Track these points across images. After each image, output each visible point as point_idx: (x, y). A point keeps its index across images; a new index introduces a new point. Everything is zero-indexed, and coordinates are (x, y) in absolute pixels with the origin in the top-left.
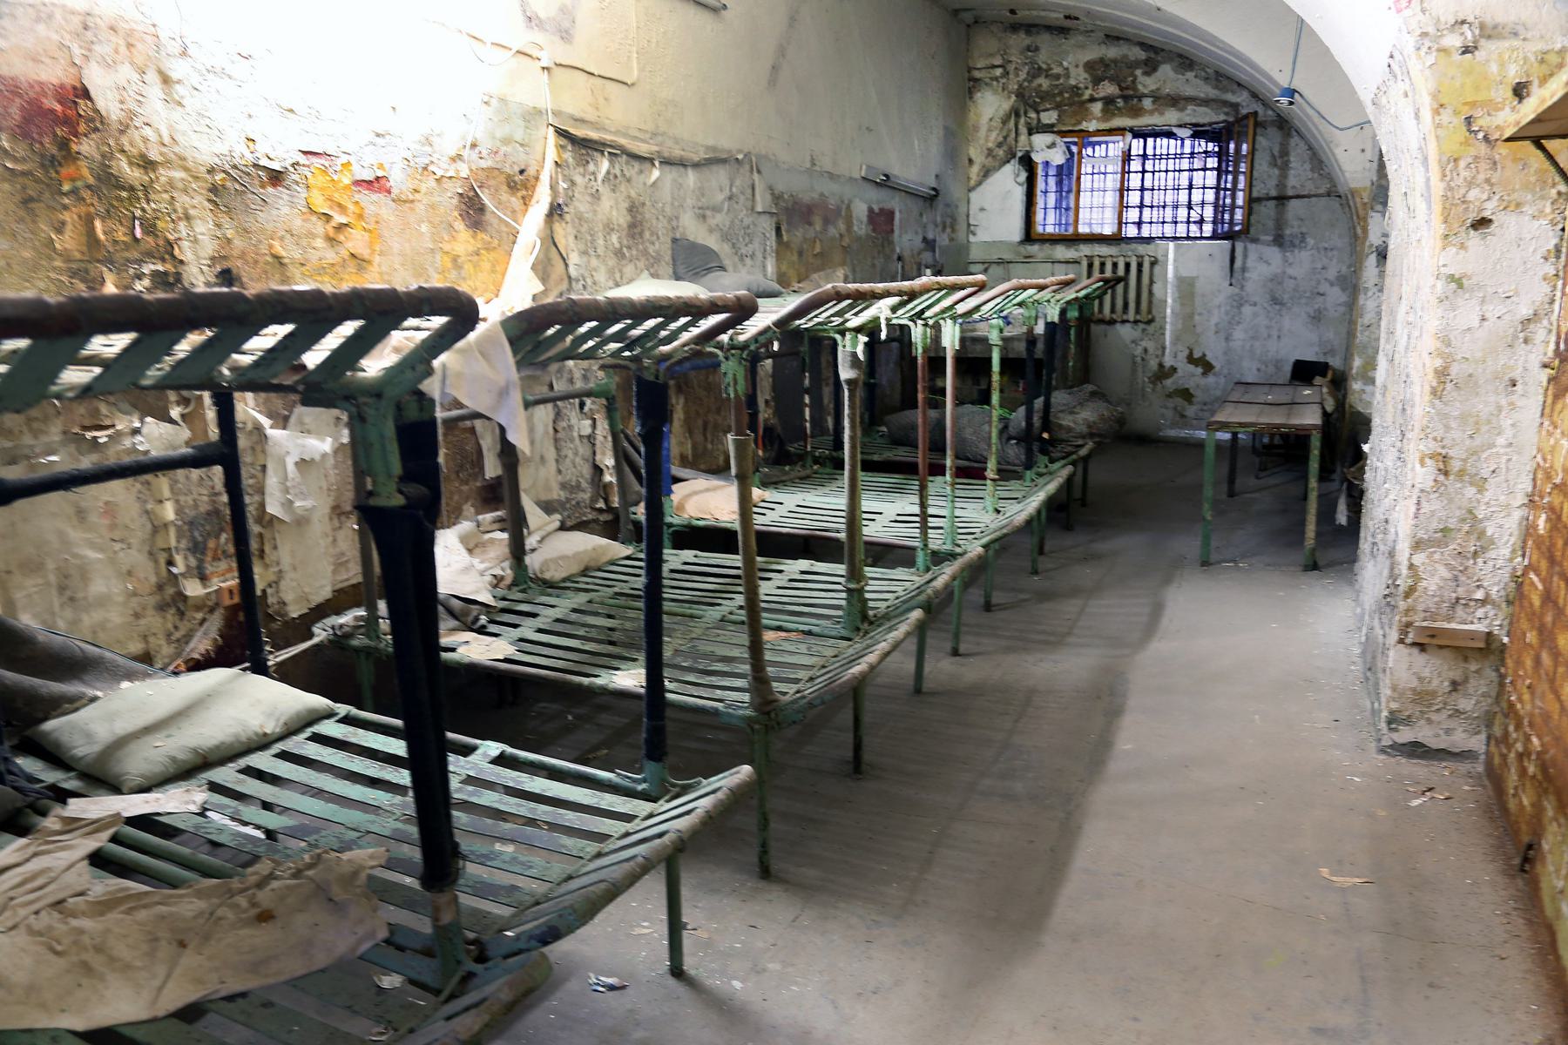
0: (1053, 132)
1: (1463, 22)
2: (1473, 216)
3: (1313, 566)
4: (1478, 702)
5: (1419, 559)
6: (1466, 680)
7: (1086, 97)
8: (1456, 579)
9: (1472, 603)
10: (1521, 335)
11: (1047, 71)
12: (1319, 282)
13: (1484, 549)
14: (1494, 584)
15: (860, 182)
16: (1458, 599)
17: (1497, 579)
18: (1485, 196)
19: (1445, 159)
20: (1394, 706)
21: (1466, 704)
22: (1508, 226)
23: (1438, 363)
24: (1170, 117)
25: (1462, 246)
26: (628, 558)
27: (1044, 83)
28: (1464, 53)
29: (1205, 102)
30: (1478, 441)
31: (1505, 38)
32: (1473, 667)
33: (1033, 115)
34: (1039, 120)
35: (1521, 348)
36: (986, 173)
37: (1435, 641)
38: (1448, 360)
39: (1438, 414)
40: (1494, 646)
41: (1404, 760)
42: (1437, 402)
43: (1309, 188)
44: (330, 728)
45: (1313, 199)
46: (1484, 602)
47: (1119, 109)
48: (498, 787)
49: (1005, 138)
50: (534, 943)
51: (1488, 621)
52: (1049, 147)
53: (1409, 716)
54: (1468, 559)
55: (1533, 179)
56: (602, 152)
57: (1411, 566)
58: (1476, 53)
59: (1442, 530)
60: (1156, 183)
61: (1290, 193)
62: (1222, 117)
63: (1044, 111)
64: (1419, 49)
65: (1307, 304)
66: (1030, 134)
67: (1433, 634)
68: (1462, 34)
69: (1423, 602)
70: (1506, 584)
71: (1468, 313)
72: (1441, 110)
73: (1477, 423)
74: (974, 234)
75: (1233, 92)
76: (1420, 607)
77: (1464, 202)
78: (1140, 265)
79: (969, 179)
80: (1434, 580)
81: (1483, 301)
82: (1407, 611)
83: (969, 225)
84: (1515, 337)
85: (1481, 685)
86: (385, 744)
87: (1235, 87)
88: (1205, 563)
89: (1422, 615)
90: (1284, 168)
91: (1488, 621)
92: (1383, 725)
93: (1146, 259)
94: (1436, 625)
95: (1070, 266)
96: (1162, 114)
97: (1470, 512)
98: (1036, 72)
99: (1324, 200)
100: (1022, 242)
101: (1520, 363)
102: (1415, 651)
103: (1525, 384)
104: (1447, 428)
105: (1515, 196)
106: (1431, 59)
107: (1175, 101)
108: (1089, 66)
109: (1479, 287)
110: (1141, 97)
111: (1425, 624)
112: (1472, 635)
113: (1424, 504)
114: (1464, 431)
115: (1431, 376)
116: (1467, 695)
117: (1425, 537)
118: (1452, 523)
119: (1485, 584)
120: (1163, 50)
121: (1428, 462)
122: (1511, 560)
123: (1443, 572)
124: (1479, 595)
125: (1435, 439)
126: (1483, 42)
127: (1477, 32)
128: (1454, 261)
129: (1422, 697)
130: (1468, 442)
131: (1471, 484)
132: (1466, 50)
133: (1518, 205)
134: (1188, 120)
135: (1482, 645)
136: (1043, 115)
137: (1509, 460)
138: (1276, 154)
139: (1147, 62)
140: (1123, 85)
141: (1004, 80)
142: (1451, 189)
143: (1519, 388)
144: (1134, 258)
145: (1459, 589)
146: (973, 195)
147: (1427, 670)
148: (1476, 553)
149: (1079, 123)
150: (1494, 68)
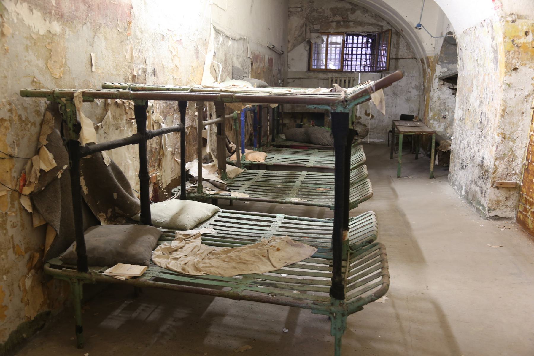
0: (318, 32)
1: (512, 14)
2: (513, 67)
3: (432, 177)
4: (513, 203)
5: (497, 163)
6: (510, 197)
7: (331, 20)
8: (507, 168)
9: (511, 175)
10: (525, 100)
11: (317, 10)
12: (409, 88)
13: (515, 159)
14: (517, 169)
15: (267, 48)
16: (508, 174)
17: (518, 168)
18: (517, 62)
19: (506, 51)
20: (490, 205)
21: (510, 204)
22: (523, 70)
23: (503, 108)
24: (359, 29)
25: (510, 75)
26: (243, 172)
27: (315, 14)
28: (512, 22)
29: (371, 24)
30: (513, 129)
31: (523, 19)
32: (512, 193)
33: (311, 26)
34: (313, 28)
35: (525, 104)
36: (294, 46)
37: (502, 186)
38: (506, 107)
39: (503, 122)
40: (517, 186)
41: (493, 221)
42: (502, 118)
43: (406, 56)
44: (220, 214)
45: (407, 60)
46: (515, 174)
47: (342, 25)
48: (364, 200)
49: (302, 34)
50: (367, 243)
51: (516, 180)
52: (317, 38)
53: (494, 208)
54: (510, 162)
55: (529, 57)
56: (220, 34)
57: (495, 165)
58: (516, 22)
59: (503, 155)
60: (347, 52)
61: (400, 57)
62: (377, 30)
63: (315, 24)
64: (500, 20)
65: (405, 95)
66: (310, 33)
67: (501, 184)
68: (512, 17)
69: (498, 175)
70: (521, 169)
71: (511, 94)
72: (506, 38)
73: (513, 124)
74: (290, 68)
75: (381, 22)
76: (497, 177)
77: (511, 63)
78: (349, 81)
79: (288, 48)
80: (501, 169)
81: (515, 90)
82: (494, 178)
83: (288, 65)
84: (524, 100)
85: (514, 197)
86: (185, 232)
87: (382, 20)
88: (399, 177)
89: (498, 179)
90: (398, 49)
91: (516, 180)
92: (487, 211)
93: (352, 78)
94: (502, 181)
95: (324, 80)
96: (356, 28)
97: (511, 149)
98: (313, 10)
99: (411, 60)
100: (307, 72)
101: (525, 107)
102: (496, 189)
103: (526, 113)
104: (505, 126)
105: (524, 62)
106: (503, 24)
107: (361, 24)
108: (332, 9)
109: (515, 87)
110: (349, 22)
111: (499, 181)
112: (512, 184)
113: (498, 147)
114: (510, 127)
115: (501, 111)
116: (510, 201)
117: (499, 156)
118: (506, 152)
119: (515, 169)
120: (357, 5)
121: (500, 135)
122: (522, 162)
123: (504, 166)
124: (513, 172)
125: (502, 129)
126: (517, 20)
127: (516, 17)
128: (508, 79)
129: (498, 202)
130: (511, 129)
131: (511, 141)
132: (513, 22)
133: (525, 64)
134: (365, 30)
135: (514, 186)
136: (315, 26)
137: (521, 134)
138: (395, 44)
139: (352, 9)
140: (344, 17)
141: (301, 13)
142: (508, 59)
143: (524, 114)
144: (347, 78)
145: (508, 171)
146: (289, 54)
147: (499, 194)
148: (512, 160)
149: (328, 29)
150: (520, 27)
